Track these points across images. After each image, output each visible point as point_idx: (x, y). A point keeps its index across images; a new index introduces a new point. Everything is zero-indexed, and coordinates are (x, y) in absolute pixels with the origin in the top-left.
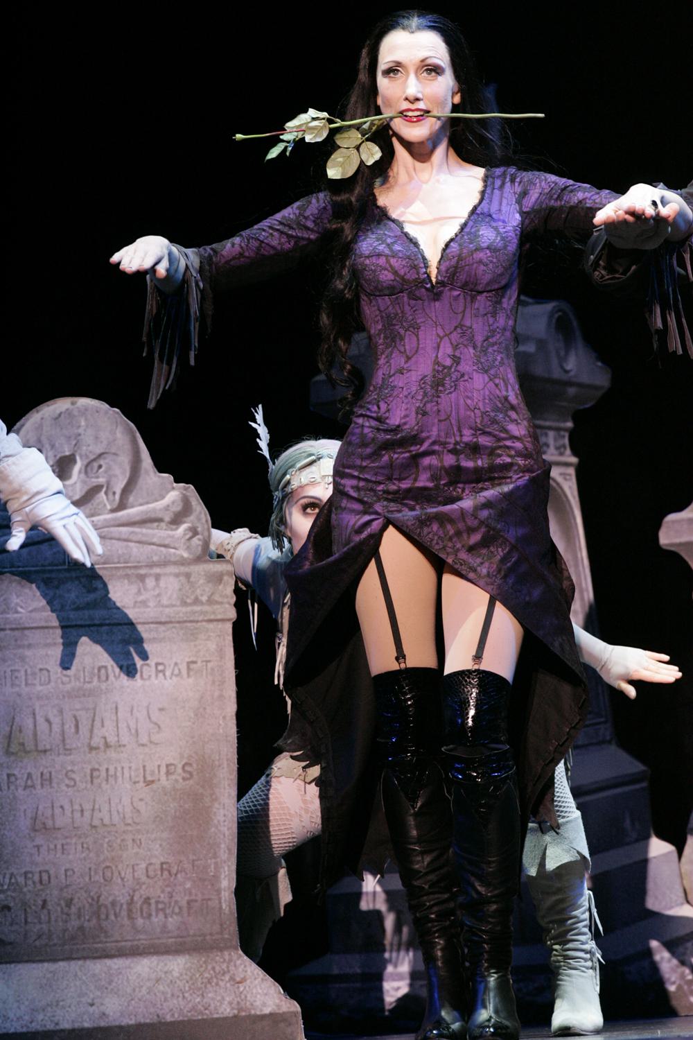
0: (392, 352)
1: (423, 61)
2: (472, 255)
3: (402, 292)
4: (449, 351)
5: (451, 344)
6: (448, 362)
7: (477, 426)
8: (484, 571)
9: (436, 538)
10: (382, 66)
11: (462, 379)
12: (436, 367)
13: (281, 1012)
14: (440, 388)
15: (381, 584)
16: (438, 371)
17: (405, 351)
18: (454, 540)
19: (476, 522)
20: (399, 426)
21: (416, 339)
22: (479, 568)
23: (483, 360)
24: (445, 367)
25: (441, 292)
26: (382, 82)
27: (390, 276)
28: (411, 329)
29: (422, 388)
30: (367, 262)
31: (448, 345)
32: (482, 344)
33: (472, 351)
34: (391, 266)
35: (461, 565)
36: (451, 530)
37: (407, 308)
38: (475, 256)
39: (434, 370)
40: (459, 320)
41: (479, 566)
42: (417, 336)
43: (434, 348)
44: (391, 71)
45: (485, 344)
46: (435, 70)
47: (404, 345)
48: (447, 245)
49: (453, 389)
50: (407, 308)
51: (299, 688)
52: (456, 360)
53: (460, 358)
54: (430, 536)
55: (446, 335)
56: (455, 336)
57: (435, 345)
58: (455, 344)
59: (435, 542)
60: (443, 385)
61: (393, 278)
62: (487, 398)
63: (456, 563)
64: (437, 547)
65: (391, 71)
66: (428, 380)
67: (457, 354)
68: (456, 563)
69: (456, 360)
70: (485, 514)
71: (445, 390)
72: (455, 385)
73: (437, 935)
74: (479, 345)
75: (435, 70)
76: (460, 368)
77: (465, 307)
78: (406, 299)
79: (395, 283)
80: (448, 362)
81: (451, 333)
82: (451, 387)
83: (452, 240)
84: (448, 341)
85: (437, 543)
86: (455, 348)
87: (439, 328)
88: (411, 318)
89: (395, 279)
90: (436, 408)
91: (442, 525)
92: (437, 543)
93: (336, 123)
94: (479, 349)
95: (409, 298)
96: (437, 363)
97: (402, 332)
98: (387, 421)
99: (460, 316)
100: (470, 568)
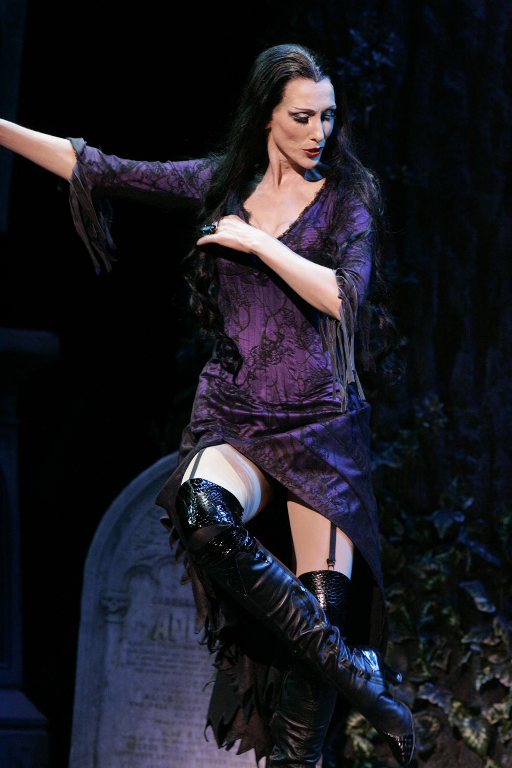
3: (237, 275)
4: (275, 329)
5: (277, 323)
6: (274, 338)
7: (300, 393)
8: (308, 488)
9: (267, 459)
12: (265, 340)
13: (276, 669)
14: (268, 359)
15: (198, 465)
17: (239, 322)
18: (283, 462)
19: (302, 448)
21: (247, 314)
22: (303, 485)
23: (303, 339)
24: (271, 342)
28: (243, 305)
29: (253, 357)
31: (273, 323)
32: (302, 325)
33: (293, 330)
35: (288, 483)
36: (281, 453)
37: (240, 287)
39: (262, 342)
41: (303, 483)
42: (248, 312)
43: (263, 325)
45: (304, 326)
47: (238, 317)
49: (278, 361)
50: (240, 287)
51: (331, 636)
52: (281, 337)
53: (283, 335)
54: (263, 457)
55: (271, 316)
56: (279, 317)
57: (263, 322)
58: (279, 323)
59: (266, 462)
60: (270, 356)
62: (308, 368)
63: (283, 481)
64: (268, 467)
66: (258, 350)
67: (282, 331)
68: (283, 481)
69: (281, 337)
70: (309, 441)
71: (272, 361)
72: (281, 358)
73: (367, 63)
74: (300, 325)
76: (285, 343)
80: (274, 338)
84: (273, 320)
85: (268, 464)
86: (279, 326)
87: (266, 309)
90: (264, 375)
91: (273, 449)
92: (268, 464)
94: (299, 329)
100: (296, 485)
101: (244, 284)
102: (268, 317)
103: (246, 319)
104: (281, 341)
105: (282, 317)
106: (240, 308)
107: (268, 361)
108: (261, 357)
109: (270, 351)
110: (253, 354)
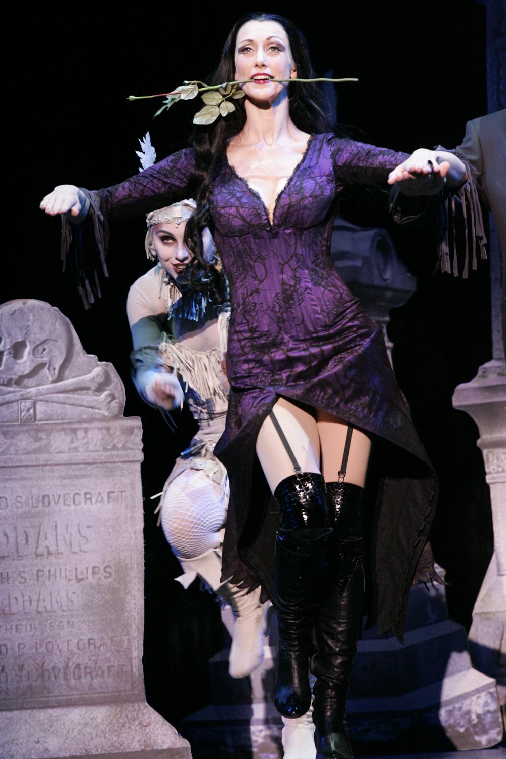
0: (245, 278)
1: (269, 39)
2: (299, 203)
10: (239, 44)
11: (306, 293)
14: (291, 302)
16: (286, 290)
17: (256, 276)
20: (267, 332)
24: (291, 286)
25: (278, 232)
26: (239, 58)
27: (240, 222)
30: (222, 211)
34: (240, 214)
38: (301, 204)
40: (293, 251)
44: (244, 50)
46: (277, 48)
48: (280, 196)
52: (298, 280)
57: (280, 271)
60: (293, 299)
61: (242, 223)
65: (244, 50)
75: (277, 48)
76: (303, 284)
77: (296, 240)
78: (252, 239)
79: (244, 227)
81: (289, 260)
82: (300, 300)
83: (282, 192)
88: (257, 252)
89: (244, 224)
93: (204, 87)
95: (254, 238)
96: (283, 283)
97: (252, 263)
98: (257, 329)
99: (293, 248)
101: (257, 241)
102: (283, 265)
103: (263, 270)
104: (299, 283)
105: (295, 262)
106: (256, 263)
107: (292, 304)
108: (285, 302)
109: (292, 295)
110: (278, 301)
